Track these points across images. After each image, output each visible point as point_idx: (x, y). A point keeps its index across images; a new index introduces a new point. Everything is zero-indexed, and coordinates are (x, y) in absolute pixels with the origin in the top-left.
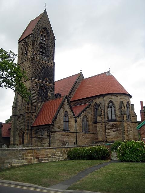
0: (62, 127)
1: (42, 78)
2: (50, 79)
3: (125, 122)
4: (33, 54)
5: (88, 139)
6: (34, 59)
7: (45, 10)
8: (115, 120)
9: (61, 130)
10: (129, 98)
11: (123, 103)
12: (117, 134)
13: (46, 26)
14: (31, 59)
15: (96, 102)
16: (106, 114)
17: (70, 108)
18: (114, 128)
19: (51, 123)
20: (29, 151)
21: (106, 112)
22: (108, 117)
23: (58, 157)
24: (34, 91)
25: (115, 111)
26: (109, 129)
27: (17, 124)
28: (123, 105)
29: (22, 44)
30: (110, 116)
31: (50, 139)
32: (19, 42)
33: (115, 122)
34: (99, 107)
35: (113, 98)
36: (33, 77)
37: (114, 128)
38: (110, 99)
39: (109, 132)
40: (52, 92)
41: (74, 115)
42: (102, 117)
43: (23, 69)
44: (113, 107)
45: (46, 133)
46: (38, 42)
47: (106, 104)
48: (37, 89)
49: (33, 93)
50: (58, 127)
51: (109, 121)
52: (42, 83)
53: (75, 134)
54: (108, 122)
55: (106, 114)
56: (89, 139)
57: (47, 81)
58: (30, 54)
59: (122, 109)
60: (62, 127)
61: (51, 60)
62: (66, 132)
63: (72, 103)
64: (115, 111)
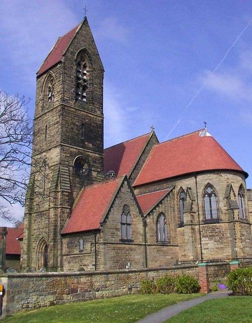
0: (119, 233)
1: (82, 144)
3: (236, 223)
7: (86, 18)
8: (218, 221)
9: (117, 239)
11: (231, 187)
12: (223, 246)
13: (87, 47)
15: (181, 187)
16: (200, 209)
18: (216, 236)
19: (98, 226)
21: (200, 205)
22: (204, 214)
24: (66, 167)
25: (217, 202)
26: (206, 236)
27: (34, 230)
28: (232, 191)
29: (43, 80)
32: (38, 77)
33: (217, 224)
35: (212, 178)
36: (63, 141)
37: (216, 236)
39: (207, 242)
40: (100, 170)
41: (141, 212)
42: (194, 214)
43: (45, 127)
44: (213, 195)
45: (88, 246)
47: (201, 191)
48: (73, 163)
50: (112, 233)
51: (206, 222)
52: (82, 154)
55: (200, 209)
57: (89, 149)
61: (97, 110)
62: (125, 244)
64: (217, 202)
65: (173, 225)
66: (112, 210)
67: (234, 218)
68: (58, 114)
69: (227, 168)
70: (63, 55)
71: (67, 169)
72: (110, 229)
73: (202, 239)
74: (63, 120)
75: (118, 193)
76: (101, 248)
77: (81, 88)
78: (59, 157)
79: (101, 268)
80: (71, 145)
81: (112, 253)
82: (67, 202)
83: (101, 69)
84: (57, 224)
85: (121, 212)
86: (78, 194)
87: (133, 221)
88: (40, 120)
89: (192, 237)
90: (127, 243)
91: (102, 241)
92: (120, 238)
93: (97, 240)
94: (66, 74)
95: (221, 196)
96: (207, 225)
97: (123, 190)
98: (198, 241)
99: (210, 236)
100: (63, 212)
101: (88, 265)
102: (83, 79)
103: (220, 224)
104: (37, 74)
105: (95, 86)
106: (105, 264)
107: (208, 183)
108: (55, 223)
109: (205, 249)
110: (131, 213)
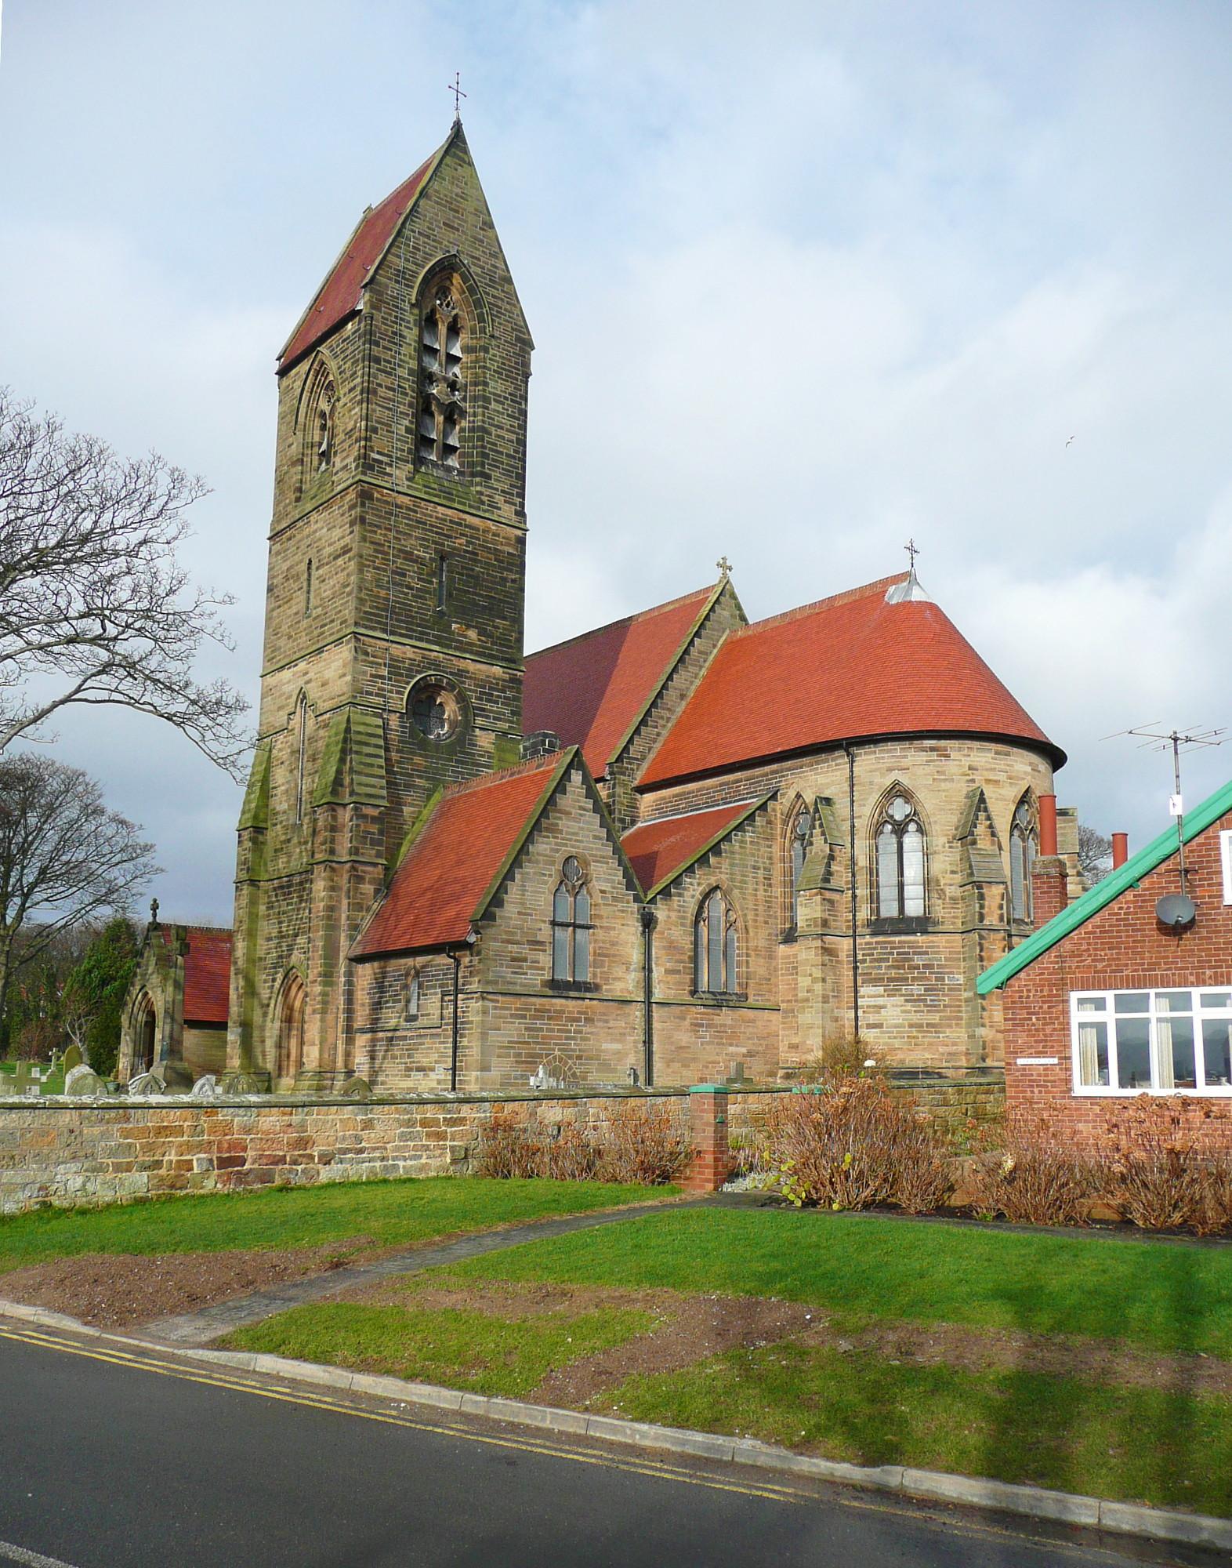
1: (434, 628)
2: (490, 636)
4: (367, 464)
5: (732, 1049)
6: (371, 498)
7: (458, 127)
8: (923, 924)
9: (536, 979)
10: (1050, 769)
11: (982, 800)
12: (935, 1018)
14: (351, 496)
15: (799, 796)
16: (862, 878)
17: (603, 833)
20: (173, 1118)
21: (862, 862)
22: (875, 899)
23: (383, 1159)
24: (375, 715)
25: (927, 855)
26: (876, 981)
28: (982, 815)
29: (299, 383)
30: (888, 893)
31: (455, 1042)
32: (282, 373)
33: (919, 937)
34: (817, 831)
35: (910, 764)
38: (890, 770)
39: (880, 1001)
42: (835, 896)
43: (304, 566)
45: (432, 1005)
46: (399, 371)
47: (866, 811)
48: (400, 702)
49: (361, 728)
51: (879, 926)
52: (436, 665)
53: (637, 1013)
54: (874, 934)
55: (862, 878)
56: (744, 1050)
58: (345, 461)
59: (974, 843)
60: (545, 959)
61: (499, 499)
62: (567, 998)
63: (649, 797)
65: (763, 933)
66: (518, 877)
67: (982, 918)
68: (347, 519)
69: (966, 726)
70: (364, 287)
71: (380, 722)
72: (509, 942)
73: (862, 991)
74: (364, 539)
75: (544, 813)
76: (473, 1010)
77: (440, 419)
78: (349, 678)
79: (468, 1082)
80: (393, 633)
81: (513, 1030)
82: (373, 843)
83: (518, 339)
84: (338, 919)
85: (552, 882)
86: (420, 812)
87: (600, 917)
88: (289, 539)
89: (824, 980)
90: (572, 994)
91: (474, 987)
92: (548, 977)
93: (460, 981)
94: (377, 361)
95: (939, 841)
96: (880, 938)
97: (563, 801)
98: (847, 996)
99: (890, 980)
100: (360, 879)
101: (432, 1069)
102: (445, 379)
103: (931, 938)
104: (279, 359)
105: (493, 405)
106: (485, 1068)
107: (896, 784)
108: (329, 918)
109: (869, 1026)
110: (596, 885)
